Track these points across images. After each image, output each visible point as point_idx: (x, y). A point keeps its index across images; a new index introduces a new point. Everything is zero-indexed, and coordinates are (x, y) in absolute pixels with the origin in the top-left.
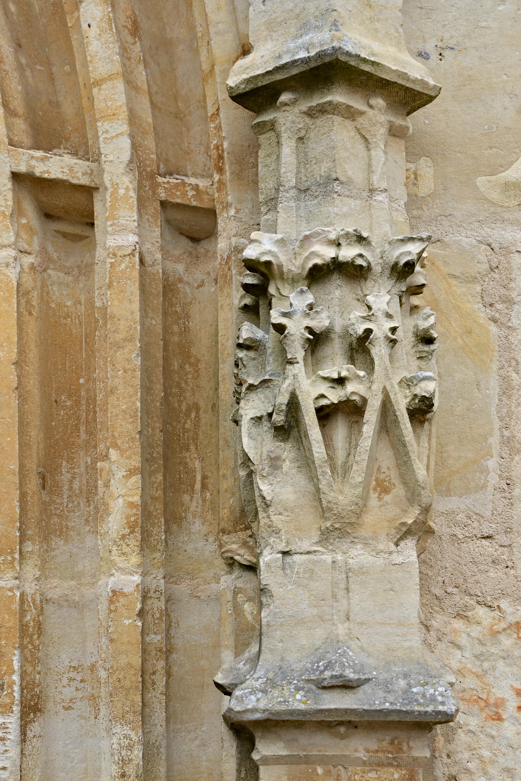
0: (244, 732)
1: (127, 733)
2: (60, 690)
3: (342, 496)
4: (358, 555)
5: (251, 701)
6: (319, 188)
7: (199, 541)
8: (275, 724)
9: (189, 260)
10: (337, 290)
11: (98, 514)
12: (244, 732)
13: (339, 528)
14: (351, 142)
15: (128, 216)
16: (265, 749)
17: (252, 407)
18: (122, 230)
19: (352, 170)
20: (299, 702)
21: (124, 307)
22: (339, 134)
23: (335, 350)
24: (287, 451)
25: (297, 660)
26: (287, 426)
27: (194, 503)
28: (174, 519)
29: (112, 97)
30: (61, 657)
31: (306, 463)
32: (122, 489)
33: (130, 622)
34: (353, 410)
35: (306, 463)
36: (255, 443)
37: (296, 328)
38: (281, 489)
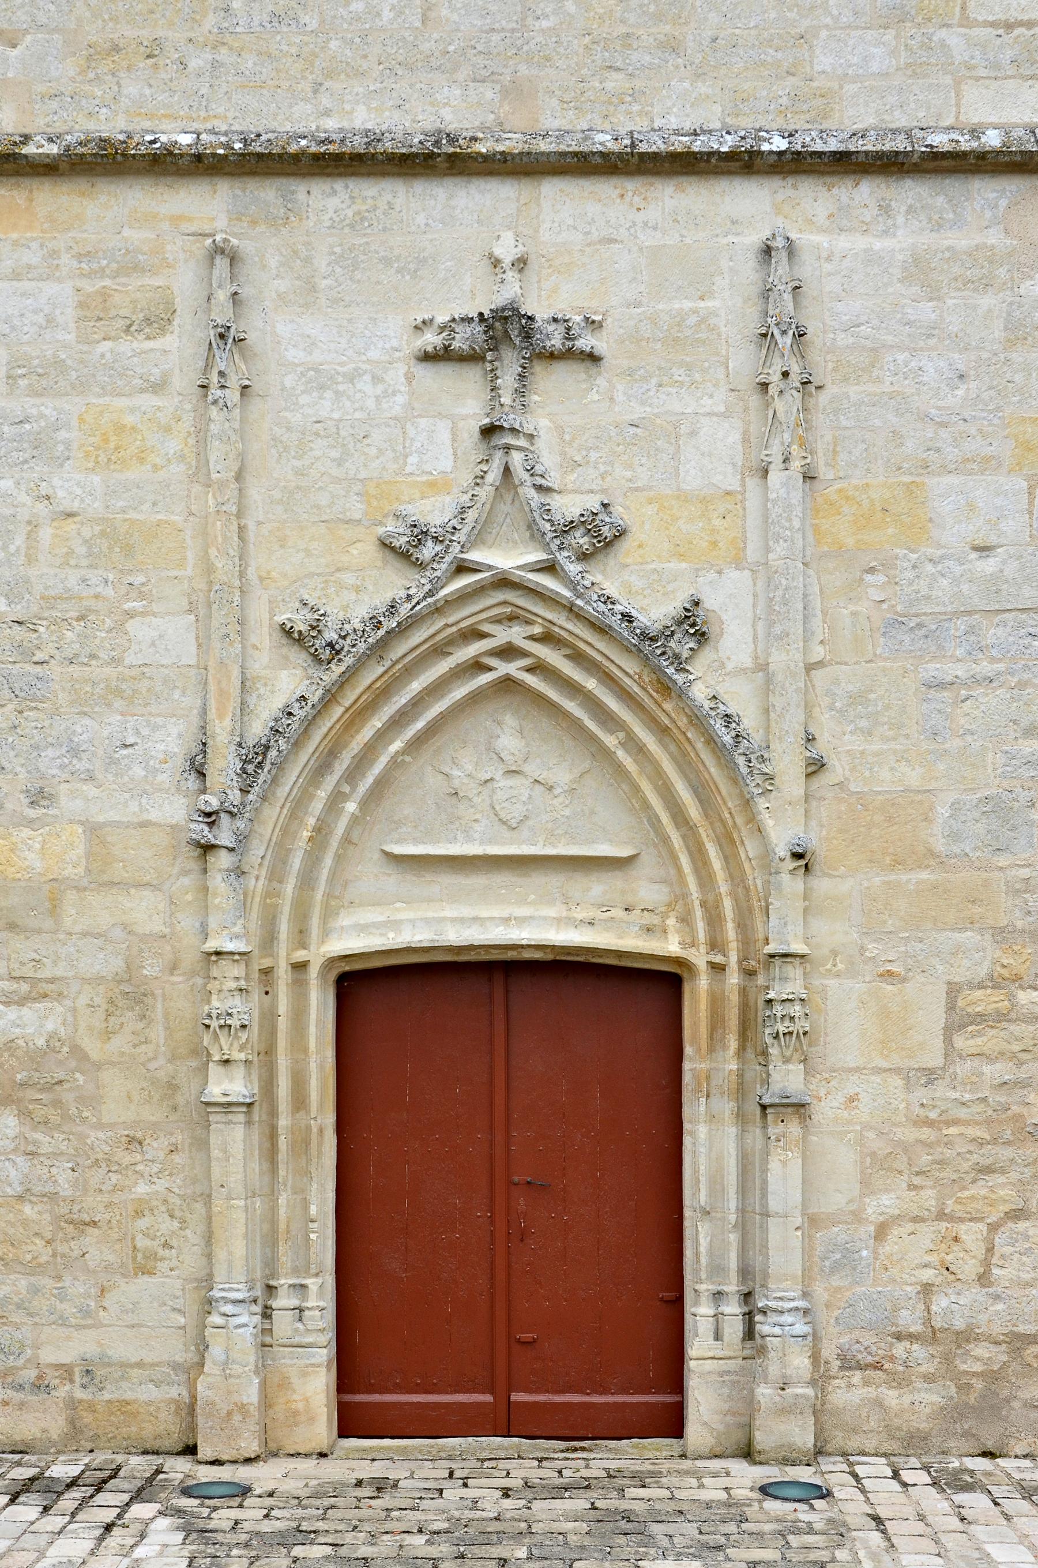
0: (764, 1107)
1: (732, 1104)
2: (713, 1091)
3: (788, 1053)
4: (791, 1067)
5: (766, 1100)
6: (784, 979)
7: (750, 1054)
8: (771, 1106)
9: (201, 149)
10: (788, 1004)
11: (725, 1048)
12: (764, 1107)
13: (787, 1060)
14: (794, 971)
15: (736, 975)
16: (769, 1111)
17: (767, 1031)
18: (733, 978)
19: (791, 975)
20: (777, 1101)
21: (735, 998)
22: (790, 967)
23: (787, 1019)
24: (776, 1042)
25: (777, 1091)
26: (776, 1037)
27: (749, 1044)
28: (744, 1049)
29: (733, 945)
30: (713, 1083)
31: (780, 1045)
32: (733, 1043)
33: (734, 1077)
34: (791, 1033)
35: (780, 1045)
36: (769, 1040)
37: (779, 1015)
38: (774, 1051)
